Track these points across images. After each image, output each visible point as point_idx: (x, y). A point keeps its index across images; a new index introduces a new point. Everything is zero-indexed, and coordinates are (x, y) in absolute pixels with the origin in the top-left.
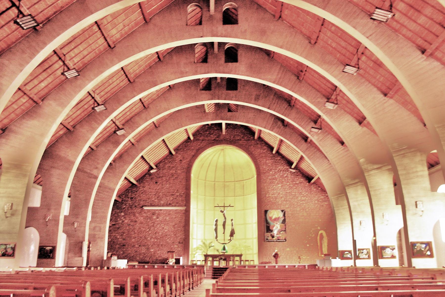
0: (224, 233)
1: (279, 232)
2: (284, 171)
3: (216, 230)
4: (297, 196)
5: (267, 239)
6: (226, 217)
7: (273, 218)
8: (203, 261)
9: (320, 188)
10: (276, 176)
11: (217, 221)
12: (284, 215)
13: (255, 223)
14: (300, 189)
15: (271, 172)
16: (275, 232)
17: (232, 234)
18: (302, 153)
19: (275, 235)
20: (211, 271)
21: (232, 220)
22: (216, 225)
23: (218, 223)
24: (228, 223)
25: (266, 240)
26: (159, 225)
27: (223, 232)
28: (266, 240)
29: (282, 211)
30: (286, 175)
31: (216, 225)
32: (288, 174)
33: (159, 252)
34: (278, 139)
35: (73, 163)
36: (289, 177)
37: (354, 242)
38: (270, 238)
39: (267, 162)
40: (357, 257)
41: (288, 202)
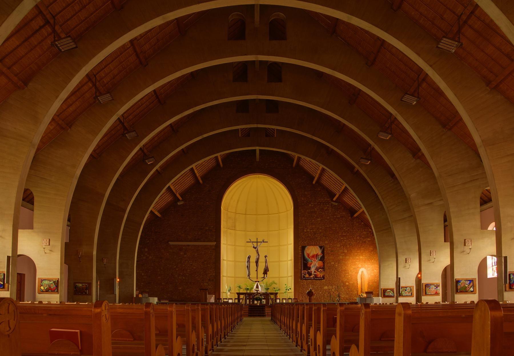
0: (257, 270)
1: (317, 269)
2: (324, 204)
3: (248, 267)
4: (337, 231)
5: (304, 277)
6: (259, 253)
7: (311, 255)
8: (235, 299)
9: (363, 223)
10: (316, 209)
11: (249, 258)
12: (323, 252)
13: (291, 260)
14: (341, 224)
15: (310, 205)
16: (313, 270)
17: (266, 271)
18: (346, 185)
19: (313, 273)
20: (248, 309)
21: (266, 257)
22: (249, 261)
23: (251, 260)
24: (262, 260)
25: (302, 277)
26: (187, 262)
27: (256, 269)
28: (302, 277)
29: (321, 247)
30: (326, 208)
31: (249, 261)
32: (328, 207)
33: (188, 290)
34: (320, 168)
35: (103, 196)
36: (330, 210)
37: (398, 280)
38: (307, 276)
39: (306, 193)
40: (400, 295)
41: (327, 238)
